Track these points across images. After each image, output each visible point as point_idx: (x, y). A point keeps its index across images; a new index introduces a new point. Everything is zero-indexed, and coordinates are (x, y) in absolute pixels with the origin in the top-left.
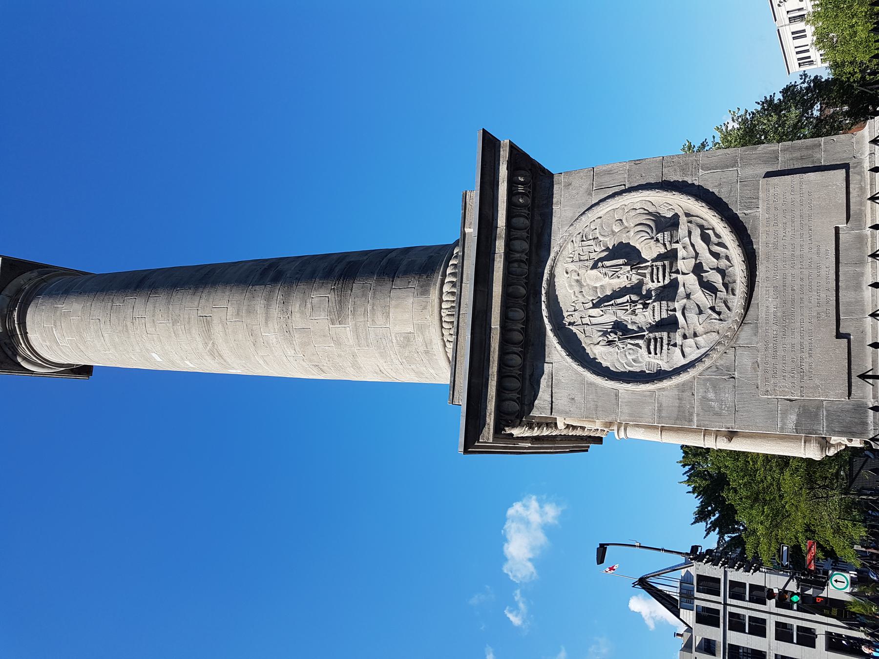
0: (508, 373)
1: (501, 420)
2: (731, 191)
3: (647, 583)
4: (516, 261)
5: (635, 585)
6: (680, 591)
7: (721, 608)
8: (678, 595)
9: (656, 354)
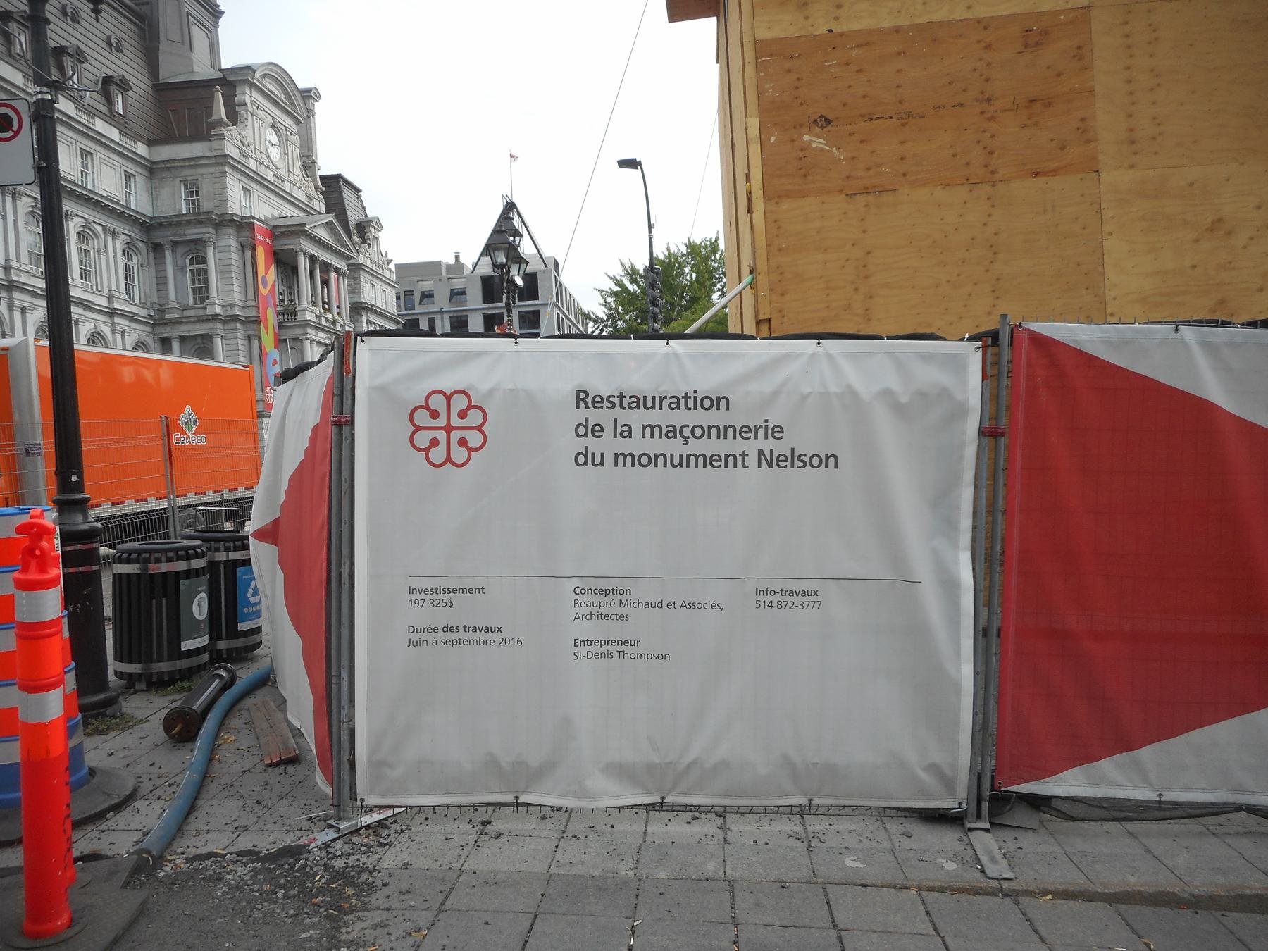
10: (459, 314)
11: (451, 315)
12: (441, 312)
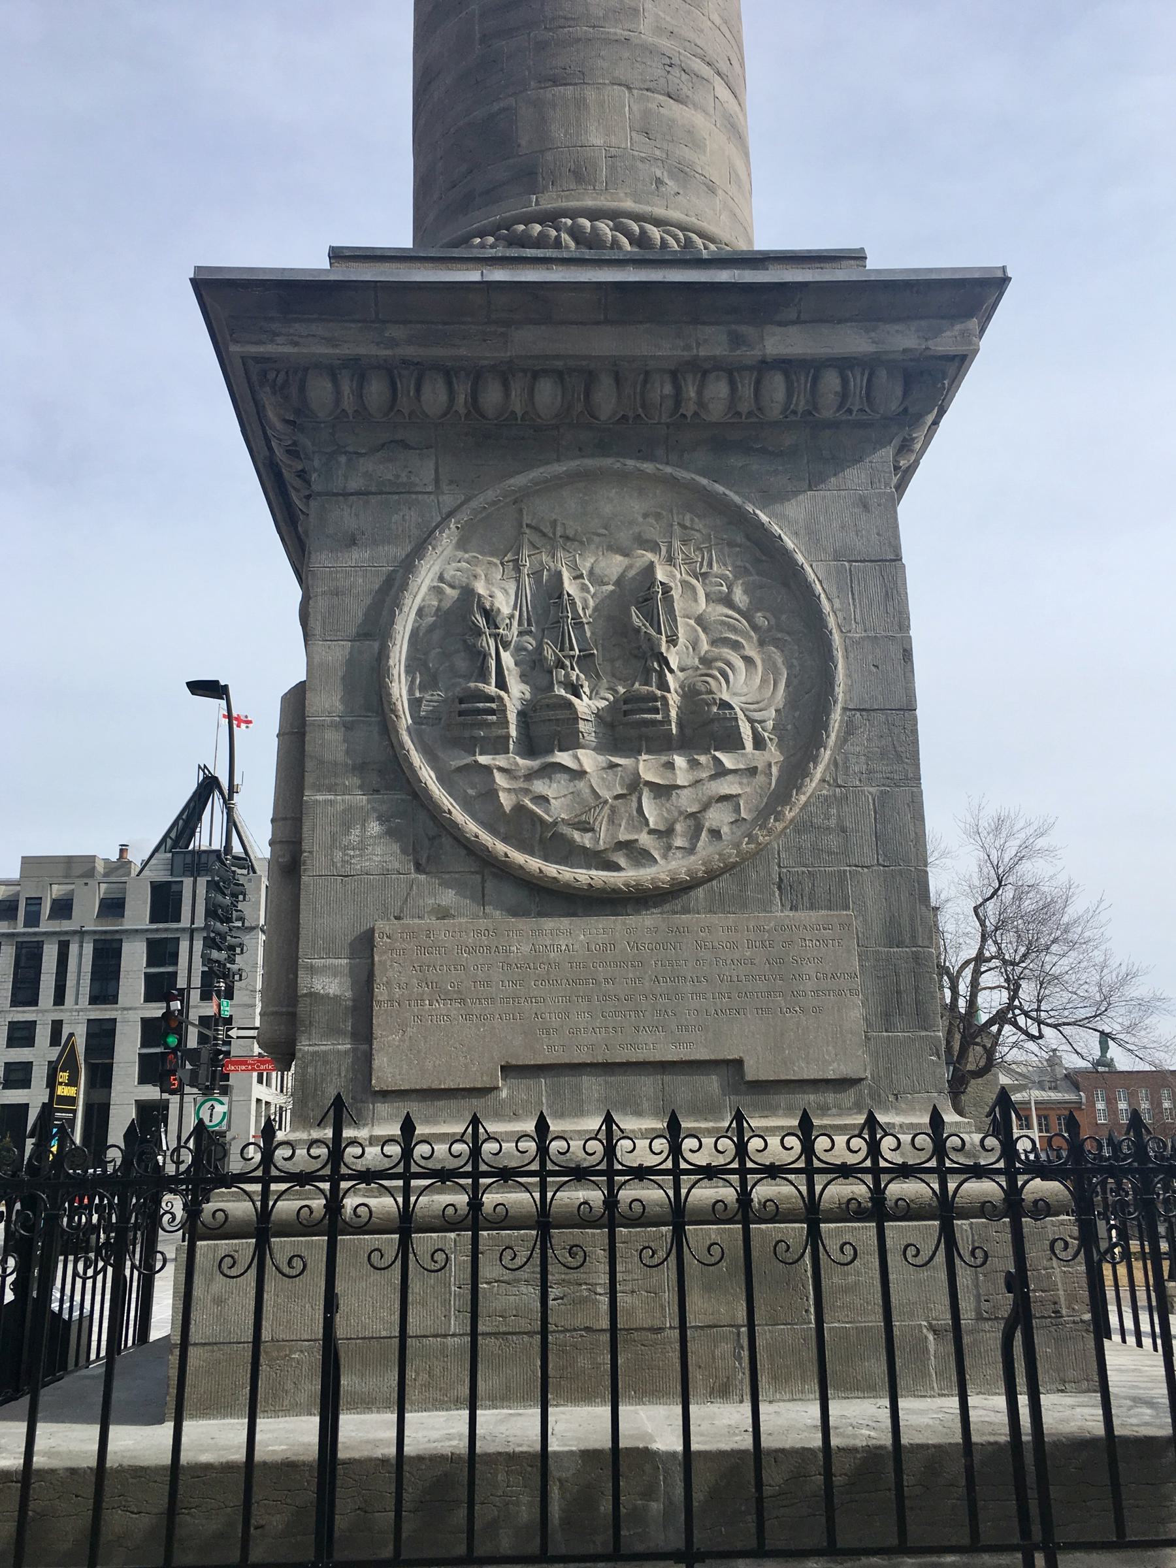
0: (401, 384)
1: (287, 373)
2: (830, 853)
3: (211, 792)
4: (678, 389)
5: (203, 771)
6: (205, 852)
7: (185, 922)
8: (197, 848)
9: (461, 714)
10: (109, 937)
11: (97, 937)
12: (81, 933)
